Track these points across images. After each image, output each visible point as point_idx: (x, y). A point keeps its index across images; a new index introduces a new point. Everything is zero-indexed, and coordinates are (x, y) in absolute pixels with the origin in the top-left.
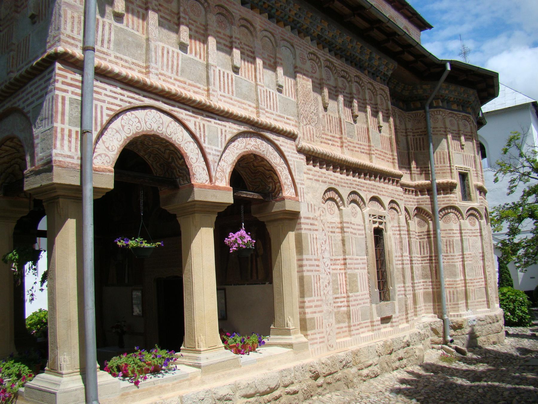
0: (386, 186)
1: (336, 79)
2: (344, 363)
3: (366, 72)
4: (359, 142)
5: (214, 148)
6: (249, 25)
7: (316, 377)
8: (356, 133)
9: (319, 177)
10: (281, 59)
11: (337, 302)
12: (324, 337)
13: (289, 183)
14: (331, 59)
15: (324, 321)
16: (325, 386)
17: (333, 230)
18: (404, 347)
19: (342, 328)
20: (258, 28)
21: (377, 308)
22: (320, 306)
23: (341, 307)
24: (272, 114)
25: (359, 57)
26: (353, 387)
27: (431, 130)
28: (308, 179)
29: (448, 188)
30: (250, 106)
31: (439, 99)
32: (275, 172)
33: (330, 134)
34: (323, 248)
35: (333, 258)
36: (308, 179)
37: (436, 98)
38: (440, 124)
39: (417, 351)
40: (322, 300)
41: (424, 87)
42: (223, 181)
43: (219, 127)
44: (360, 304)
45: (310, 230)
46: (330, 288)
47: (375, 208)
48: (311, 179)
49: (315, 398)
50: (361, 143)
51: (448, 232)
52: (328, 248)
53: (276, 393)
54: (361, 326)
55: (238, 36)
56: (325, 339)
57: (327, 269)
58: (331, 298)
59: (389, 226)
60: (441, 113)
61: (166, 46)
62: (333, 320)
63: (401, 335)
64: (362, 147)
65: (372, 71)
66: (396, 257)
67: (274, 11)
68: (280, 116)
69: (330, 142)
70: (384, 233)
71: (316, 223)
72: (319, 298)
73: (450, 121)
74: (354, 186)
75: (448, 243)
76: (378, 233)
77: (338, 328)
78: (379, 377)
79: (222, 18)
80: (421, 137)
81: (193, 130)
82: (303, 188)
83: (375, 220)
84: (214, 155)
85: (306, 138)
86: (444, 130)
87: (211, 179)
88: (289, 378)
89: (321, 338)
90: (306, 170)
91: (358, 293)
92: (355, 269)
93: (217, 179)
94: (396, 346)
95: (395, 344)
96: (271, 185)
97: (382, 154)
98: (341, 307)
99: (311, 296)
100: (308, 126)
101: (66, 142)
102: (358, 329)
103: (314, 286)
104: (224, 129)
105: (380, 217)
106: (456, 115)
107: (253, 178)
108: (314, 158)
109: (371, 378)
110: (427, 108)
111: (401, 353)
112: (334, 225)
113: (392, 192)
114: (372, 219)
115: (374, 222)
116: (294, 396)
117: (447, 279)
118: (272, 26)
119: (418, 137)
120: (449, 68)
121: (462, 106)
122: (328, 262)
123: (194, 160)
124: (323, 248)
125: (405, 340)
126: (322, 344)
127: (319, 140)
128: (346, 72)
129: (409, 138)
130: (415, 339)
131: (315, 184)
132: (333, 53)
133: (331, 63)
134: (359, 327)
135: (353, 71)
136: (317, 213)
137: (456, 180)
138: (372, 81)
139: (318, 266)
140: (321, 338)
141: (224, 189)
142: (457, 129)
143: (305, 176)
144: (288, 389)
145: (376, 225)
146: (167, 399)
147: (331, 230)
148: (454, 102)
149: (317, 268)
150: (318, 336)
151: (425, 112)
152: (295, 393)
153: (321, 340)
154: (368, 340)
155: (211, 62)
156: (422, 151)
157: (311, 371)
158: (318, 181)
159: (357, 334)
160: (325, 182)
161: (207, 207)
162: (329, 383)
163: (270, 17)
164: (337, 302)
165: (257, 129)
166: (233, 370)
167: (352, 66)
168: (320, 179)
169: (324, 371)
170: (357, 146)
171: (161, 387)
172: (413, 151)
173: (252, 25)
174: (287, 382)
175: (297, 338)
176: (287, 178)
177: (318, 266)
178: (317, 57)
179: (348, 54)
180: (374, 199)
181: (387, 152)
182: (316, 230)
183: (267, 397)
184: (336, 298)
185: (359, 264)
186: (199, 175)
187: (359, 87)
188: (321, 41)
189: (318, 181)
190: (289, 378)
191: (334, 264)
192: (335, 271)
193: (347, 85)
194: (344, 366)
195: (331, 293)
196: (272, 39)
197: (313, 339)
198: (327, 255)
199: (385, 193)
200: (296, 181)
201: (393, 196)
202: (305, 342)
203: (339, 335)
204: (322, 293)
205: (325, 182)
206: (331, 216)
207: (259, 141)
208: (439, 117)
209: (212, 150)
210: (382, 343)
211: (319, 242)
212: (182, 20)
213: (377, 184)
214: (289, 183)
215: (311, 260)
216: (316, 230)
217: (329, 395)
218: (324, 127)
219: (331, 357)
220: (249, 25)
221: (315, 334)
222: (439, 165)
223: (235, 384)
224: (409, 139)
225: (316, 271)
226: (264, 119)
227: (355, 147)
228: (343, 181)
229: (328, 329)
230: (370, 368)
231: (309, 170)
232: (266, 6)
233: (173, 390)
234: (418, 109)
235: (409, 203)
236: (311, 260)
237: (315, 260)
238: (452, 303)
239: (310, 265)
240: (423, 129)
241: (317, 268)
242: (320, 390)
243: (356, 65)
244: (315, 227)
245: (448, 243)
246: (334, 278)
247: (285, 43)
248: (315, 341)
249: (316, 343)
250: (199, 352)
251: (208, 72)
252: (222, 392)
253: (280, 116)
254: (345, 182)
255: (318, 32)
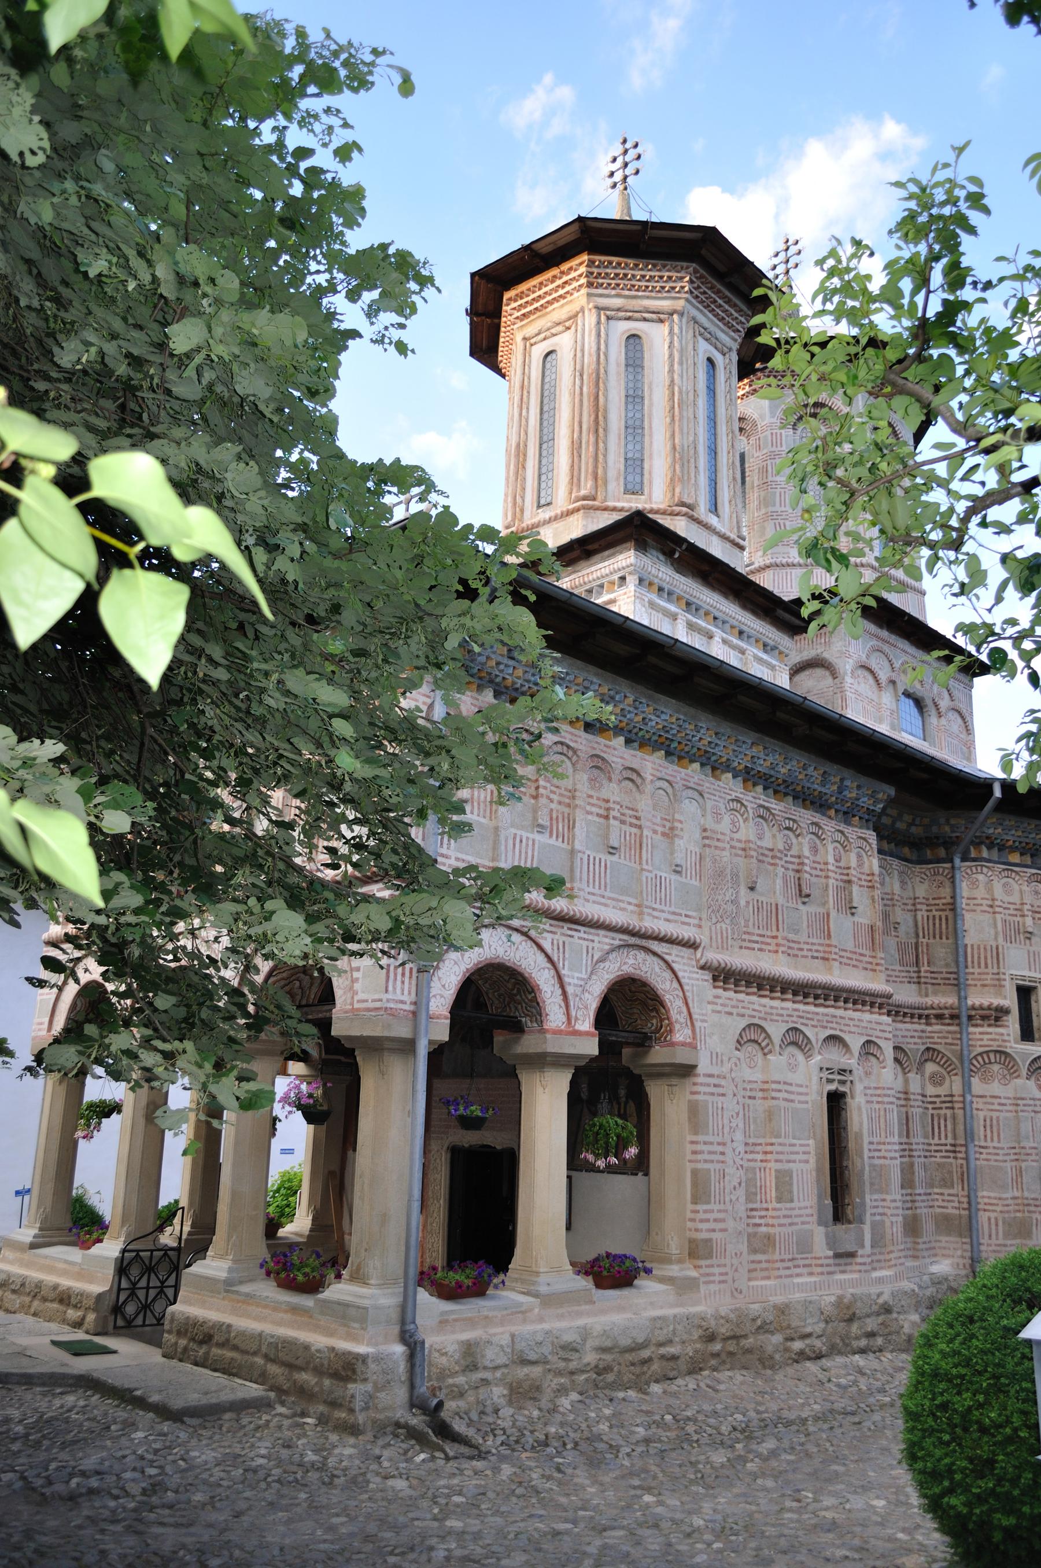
0: (857, 1015)
1: (774, 836)
2: (759, 1322)
3: (832, 812)
4: (810, 940)
5: (576, 975)
6: (634, 776)
7: (711, 1338)
8: (805, 924)
9: (733, 1007)
10: (681, 822)
11: (754, 1217)
12: (726, 1274)
13: (682, 1020)
14: (767, 804)
15: (729, 1247)
16: (723, 1356)
17: (753, 1094)
18: (878, 1314)
19: (760, 1262)
20: (649, 778)
21: (827, 1235)
22: (723, 1220)
23: (760, 1225)
24: (663, 911)
25: (820, 789)
26: (772, 1368)
27: (963, 903)
28: (713, 1011)
29: (998, 1015)
30: (630, 903)
31: (981, 843)
32: (662, 1004)
33: (757, 931)
34: (734, 1125)
35: (751, 1141)
36: (713, 1011)
37: (977, 843)
38: (980, 893)
39: (906, 1326)
40: (726, 1211)
41: (953, 822)
42: (586, 1023)
43: (585, 943)
44: (796, 1224)
45: (713, 1094)
46: (741, 1192)
47: (835, 1057)
48: (719, 1012)
49: (706, 1373)
50: (815, 941)
51: (989, 1100)
52: (741, 1125)
53: (646, 1354)
54: (796, 1262)
55: (618, 799)
56: (729, 1278)
57: (737, 1160)
58: (743, 1208)
59: (859, 1087)
60: (985, 870)
61: (519, 833)
62: (744, 1248)
63: (874, 1290)
64: (815, 948)
65: (845, 809)
66: (871, 1143)
67: (674, 745)
68: (674, 913)
69: (756, 946)
70: (848, 1099)
71: (723, 1082)
72: (722, 1207)
73: (1005, 885)
74: (794, 1019)
75: (988, 1123)
76: (836, 1102)
77: (753, 1262)
78: (824, 1360)
79: (596, 772)
80: (944, 914)
81: (549, 951)
82: (702, 1022)
83: (831, 1077)
84: (576, 985)
85: (714, 944)
86: (990, 903)
87: (568, 1018)
88: (665, 1331)
89: (721, 1274)
90: (711, 999)
91: (792, 1205)
92: (789, 1161)
93: (577, 1019)
94: (860, 1309)
95: (859, 1304)
96: (654, 1021)
97: (854, 957)
98: (760, 1225)
99: (709, 1203)
100: (718, 925)
101: (399, 983)
102: (788, 1268)
103: (714, 1187)
104: (591, 945)
105: (842, 1071)
106: (1017, 873)
107: (629, 1011)
108: (724, 976)
109: (809, 1359)
110: (957, 861)
111: (871, 1324)
112: (754, 1086)
113: (869, 1025)
114: (825, 1075)
115: (830, 1081)
116: (671, 1364)
117: (985, 1193)
118: (671, 769)
119: (937, 914)
120: (998, 793)
121: (1032, 856)
122: (741, 1148)
123: (548, 995)
124: (734, 1125)
125: (881, 1301)
126: (722, 1286)
127: (737, 944)
128: (794, 821)
129: (919, 914)
130: (903, 1303)
131: (726, 1020)
132: (771, 791)
133: (768, 809)
134: (790, 1264)
135: (806, 816)
136: (725, 1069)
137: (1010, 1000)
138: (842, 827)
139: (723, 1153)
140: (721, 1274)
141: (587, 1034)
142: (1018, 902)
143: (710, 1007)
144: (662, 1351)
145: (832, 1087)
146: (495, 1335)
147: (749, 1093)
148: (1013, 849)
149: (721, 1158)
150: (716, 1270)
151: (953, 868)
152: (674, 1358)
153: (722, 1278)
154: (807, 1288)
155: (578, 846)
156: (944, 940)
157: (700, 1327)
158: (731, 1014)
159: (787, 1276)
160: (743, 1016)
161: (558, 1061)
162: (731, 1354)
163: (669, 754)
164: (754, 1217)
165: (637, 938)
166: (583, 1307)
167: (805, 807)
168: (735, 1011)
169: (723, 1330)
170: (806, 947)
171: (487, 1317)
172: (925, 941)
173: (639, 774)
174: (661, 1339)
175: (682, 1270)
176: (680, 1013)
177: (723, 1153)
178: (742, 804)
179: (799, 788)
180: (833, 1039)
181: (864, 952)
182: (723, 1095)
183: (629, 1357)
184: (752, 1210)
185: (797, 1153)
186: (554, 1016)
187: (818, 842)
188: (750, 777)
189: (731, 1014)
190: (665, 1331)
191: (752, 1152)
192: (752, 1164)
193: (794, 841)
194: (759, 1328)
195: (743, 1199)
196: (670, 790)
197: (708, 1275)
198: (739, 1136)
199: (853, 1029)
200: (695, 1017)
201: (871, 1032)
202: (695, 1279)
203: (754, 1274)
204: (727, 1199)
205: (743, 1016)
206: (749, 1070)
207: (641, 955)
208: (981, 877)
209: (572, 978)
210: (833, 1299)
211: (727, 1115)
212: (541, 791)
213: (840, 1012)
214: (682, 1020)
215: (711, 1143)
216: (723, 1095)
217: (729, 1373)
218: (747, 921)
219: (736, 1309)
220: (634, 776)
221: (712, 1266)
222: (977, 970)
223: (585, 1328)
224: (919, 918)
225: (718, 1162)
226: (649, 924)
227: (802, 950)
228: (774, 1011)
229: (735, 1261)
230: (808, 1341)
231: (717, 997)
232: (663, 740)
233: (502, 1324)
234: (939, 861)
235: (912, 1040)
236: (711, 1143)
237: (719, 1144)
238: (994, 1241)
239: (710, 1153)
240: (949, 900)
241: (721, 1158)
242: (713, 1362)
243: (812, 803)
244: (720, 1090)
245: (988, 1123)
246: (750, 1176)
247: (690, 791)
248: (712, 1278)
249: (713, 1282)
250: (538, 1273)
251: (572, 862)
252: (568, 1338)
253: (674, 913)
254: (778, 1013)
255: (746, 762)
